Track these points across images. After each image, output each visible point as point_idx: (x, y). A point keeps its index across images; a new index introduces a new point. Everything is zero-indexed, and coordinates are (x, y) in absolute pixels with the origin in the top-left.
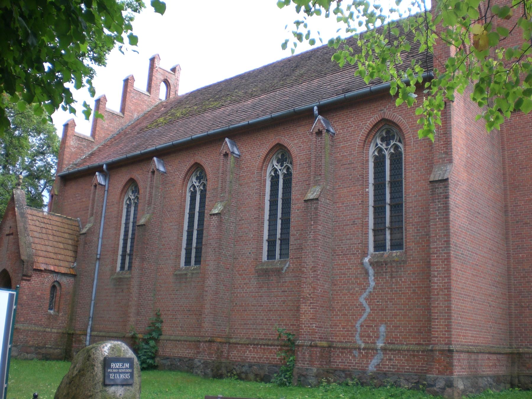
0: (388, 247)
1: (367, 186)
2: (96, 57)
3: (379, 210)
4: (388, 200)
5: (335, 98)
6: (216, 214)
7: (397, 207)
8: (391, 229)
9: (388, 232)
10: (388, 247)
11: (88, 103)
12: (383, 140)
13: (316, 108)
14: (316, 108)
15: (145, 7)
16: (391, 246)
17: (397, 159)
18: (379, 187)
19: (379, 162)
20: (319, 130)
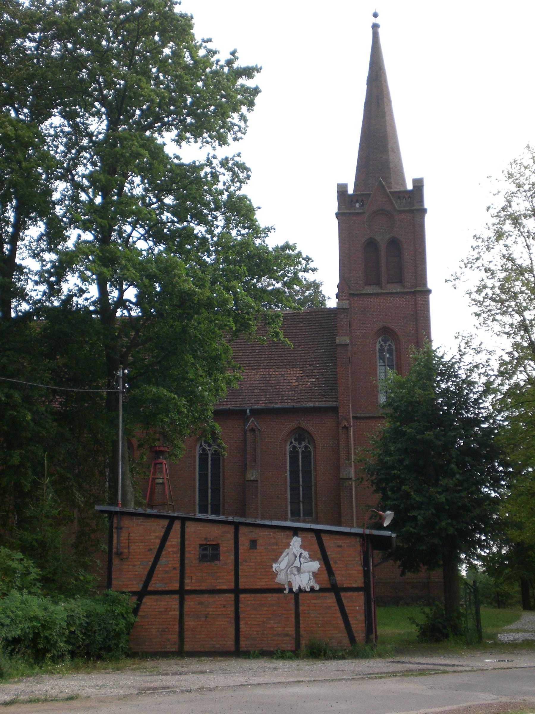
0: (302, 515)
1: (286, 472)
2: (49, 244)
3: (294, 489)
4: (301, 483)
5: (291, 405)
6: (160, 483)
7: (307, 487)
8: (303, 502)
9: (301, 505)
10: (302, 515)
11: (209, 43)
12: (295, 440)
13: (248, 410)
14: (248, 410)
15: (173, 140)
16: (304, 514)
17: (307, 455)
18: (294, 474)
19: (294, 455)
20: (252, 428)
